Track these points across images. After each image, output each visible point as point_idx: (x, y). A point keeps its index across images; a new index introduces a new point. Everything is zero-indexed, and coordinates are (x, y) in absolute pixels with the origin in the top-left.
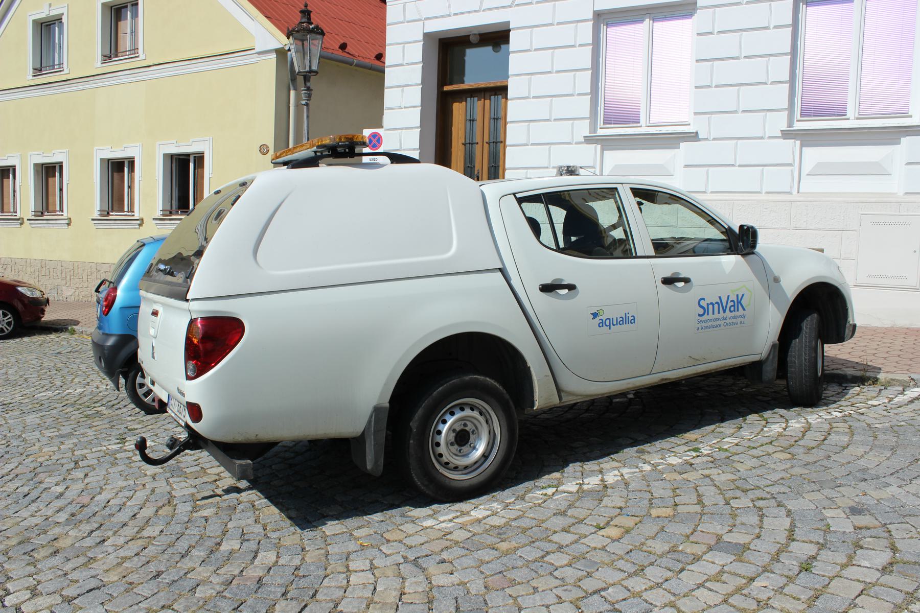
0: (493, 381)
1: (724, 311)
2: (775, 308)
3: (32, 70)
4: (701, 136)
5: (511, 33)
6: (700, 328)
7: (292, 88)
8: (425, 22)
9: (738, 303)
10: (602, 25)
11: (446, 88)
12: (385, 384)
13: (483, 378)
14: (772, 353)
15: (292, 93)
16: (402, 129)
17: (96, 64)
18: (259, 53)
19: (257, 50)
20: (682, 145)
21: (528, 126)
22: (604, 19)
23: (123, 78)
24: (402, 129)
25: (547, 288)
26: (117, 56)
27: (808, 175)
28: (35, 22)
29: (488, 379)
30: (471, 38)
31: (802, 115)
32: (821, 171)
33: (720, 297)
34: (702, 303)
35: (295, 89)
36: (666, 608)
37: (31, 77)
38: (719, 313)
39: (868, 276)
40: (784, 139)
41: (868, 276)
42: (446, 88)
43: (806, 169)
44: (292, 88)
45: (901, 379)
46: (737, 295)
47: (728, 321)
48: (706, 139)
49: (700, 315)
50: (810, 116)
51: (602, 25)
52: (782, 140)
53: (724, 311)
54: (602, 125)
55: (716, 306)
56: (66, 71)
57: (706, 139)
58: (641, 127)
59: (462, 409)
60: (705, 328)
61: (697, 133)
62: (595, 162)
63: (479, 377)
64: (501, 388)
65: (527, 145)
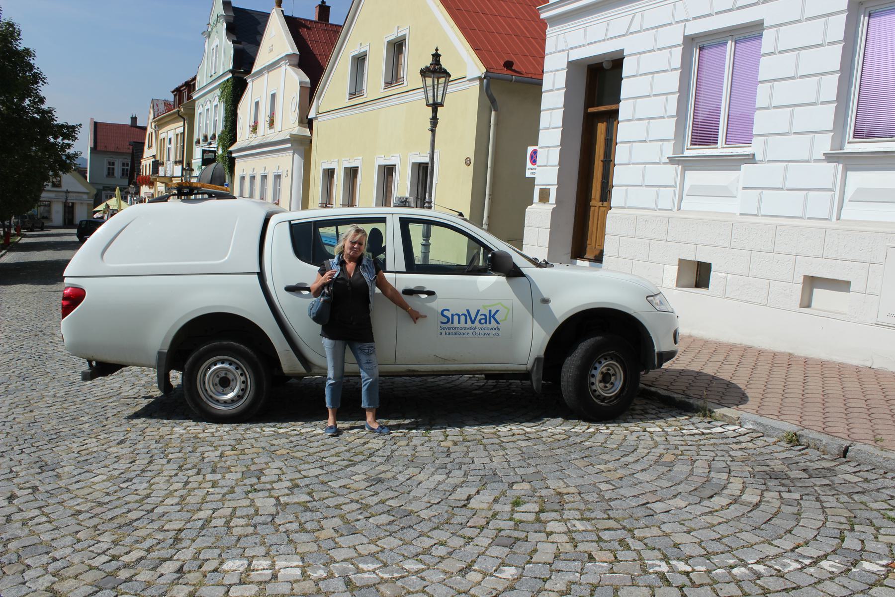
0: (246, 349)
1: (473, 322)
2: (540, 328)
3: (383, 84)
4: (757, 158)
5: (626, 62)
6: (444, 334)
7: (492, 110)
8: (570, 51)
9: (491, 316)
10: (862, 16)
11: (591, 110)
12: (165, 338)
13: (238, 344)
14: (536, 365)
15: (493, 113)
16: (549, 147)
17: (381, 91)
18: (470, 80)
19: (468, 78)
20: (743, 167)
21: (631, 147)
22: (866, 8)
23: (394, 101)
24: (549, 147)
25: (289, 289)
26: (396, 82)
27: (850, 201)
28: (353, 57)
29: (242, 346)
30: (604, 65)
31: (854, 137)
32: (865, 197)
33: (468, 311)
34: (445, 313)
35: (495, 110)
36: (369, 557)
37: (347, 100)
38: (466, 323)
39: (889, 315)
40: (828, 162)
41: (889, 315)
42: (591, 110)
43: (849, 194)
44: (492, 110)
45: (730, 415)
46: (490, 311)
47: (478, 331)
48: (761, 162)
49: (442, 323)
50: (862, 138)
51: (862, 16)
52: (825, 164)
53: (473, 322)
54: (689, 147)
55: (463, 318)
56: (406, 84)
57: (761, 162)
58: (717, 148)
59: (230, 364)
60: (449, 334)
61: (754, 155)
62: (676, 183)
63: (234, 343)
64: (252, 353)
65: (660, 164)
